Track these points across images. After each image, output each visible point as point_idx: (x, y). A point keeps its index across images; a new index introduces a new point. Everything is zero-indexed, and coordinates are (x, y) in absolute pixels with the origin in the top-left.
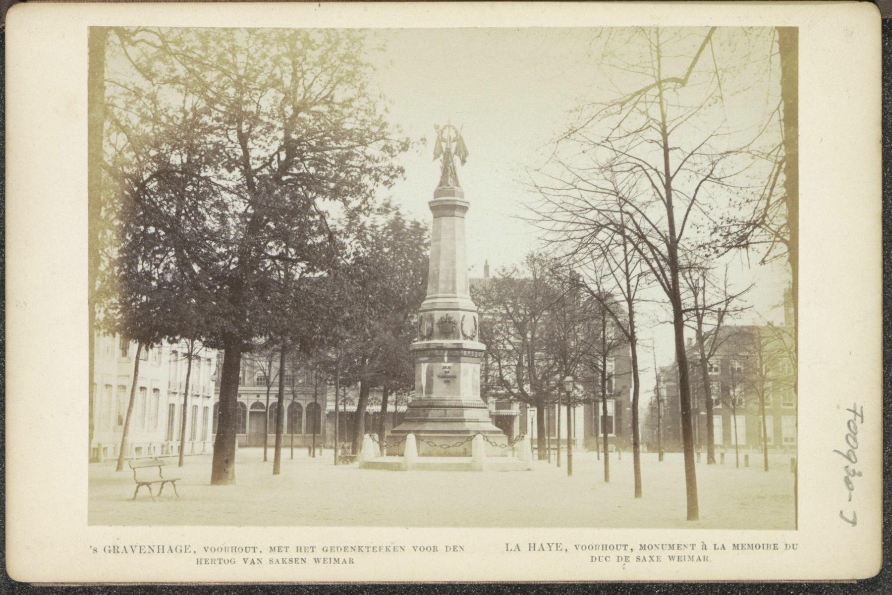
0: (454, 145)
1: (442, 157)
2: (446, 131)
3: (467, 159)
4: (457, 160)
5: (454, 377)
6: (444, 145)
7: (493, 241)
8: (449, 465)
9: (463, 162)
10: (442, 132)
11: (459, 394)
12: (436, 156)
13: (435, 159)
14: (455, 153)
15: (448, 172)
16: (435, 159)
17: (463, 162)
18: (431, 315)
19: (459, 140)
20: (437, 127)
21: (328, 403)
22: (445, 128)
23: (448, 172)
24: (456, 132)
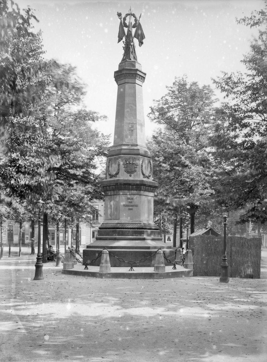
0: (134, 30)
1: (124, 39)
2: (128, 18)
3: (144, 41)
4: (136, 41)
5: (137, 206)
6: (126, 30)
7: (135, 22)
8: (115, 248)
9: (141, 43)
10: (125, 19)
11: (140, 219)
12: (120, 39)
13: (119, 41)
14: (135, 36)
15: (128, 50)
16: (119, 41)
17: (141, 43)
18: (166, 232)
19: (138, 26)
20: (119, 15)
21: (62, 236)
22: (127, 15)
23: (128, 50)
24: (136, 20)
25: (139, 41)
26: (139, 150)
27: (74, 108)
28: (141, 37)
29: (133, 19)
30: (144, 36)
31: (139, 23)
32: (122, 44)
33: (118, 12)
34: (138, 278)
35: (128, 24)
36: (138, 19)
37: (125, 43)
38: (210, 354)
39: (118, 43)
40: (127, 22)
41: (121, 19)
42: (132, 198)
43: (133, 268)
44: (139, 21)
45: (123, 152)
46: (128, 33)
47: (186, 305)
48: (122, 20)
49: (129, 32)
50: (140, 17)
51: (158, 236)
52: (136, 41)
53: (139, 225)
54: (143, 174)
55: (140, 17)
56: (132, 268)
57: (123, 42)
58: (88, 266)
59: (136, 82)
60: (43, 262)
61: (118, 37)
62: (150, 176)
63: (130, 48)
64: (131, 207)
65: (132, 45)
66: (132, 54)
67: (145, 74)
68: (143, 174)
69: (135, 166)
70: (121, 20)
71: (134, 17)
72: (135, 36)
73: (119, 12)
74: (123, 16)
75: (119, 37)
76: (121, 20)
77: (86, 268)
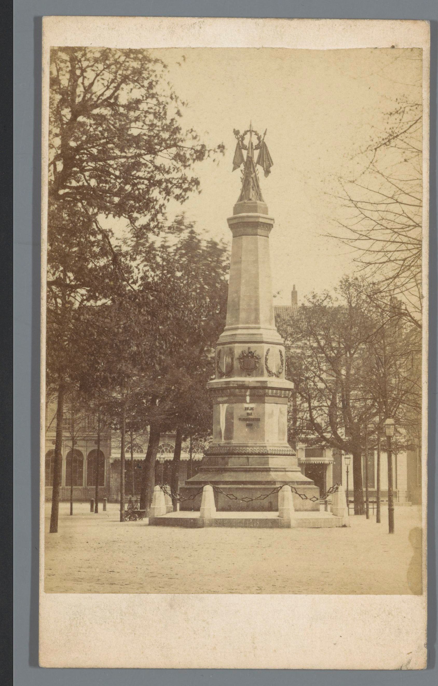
0: (256, 153)
1: (242, 167)
2: (247, 137)
3: (272, 169)
4: (260, 170)
6: (245, 153)
9: (267, 172)
10: (243, 138)
12: (236, 166)
13: (234, 169)
14: (258, 162)
15: (249, 183)
16: (234, 169)
17: (267, 172)
19: (262, 146)
24: (259, 138)
25: (264, 169)
26: (261, 334)
27: (156, 270)
28: (266, 160)
30: (272, 162)
31: (264, 143)
32: (239, 174)
33: (234, 130)
34: (149, 498)
37: (243, 172)
38: (120, 89)
40: (246, 142)
42: (251, 408)
45: (238, 339)
46: (247, 160)
47: (180, 506)
49: (250, 159)
50: (265, 134)
52: (260, 170)
55: (265, 134)
57: (241, 171)
59: (258, 234)
61: (233, 163)
62: (280, 373)
63: (249, 182)
64: (251, 423)
65: (252, 178)
66: (253, 190)
67: (273, 220)
69: (257, 360)
71: (256, 134)
72: (258, 162)
73: (236, 130)
74: (241, 133)
75: (234, 163)
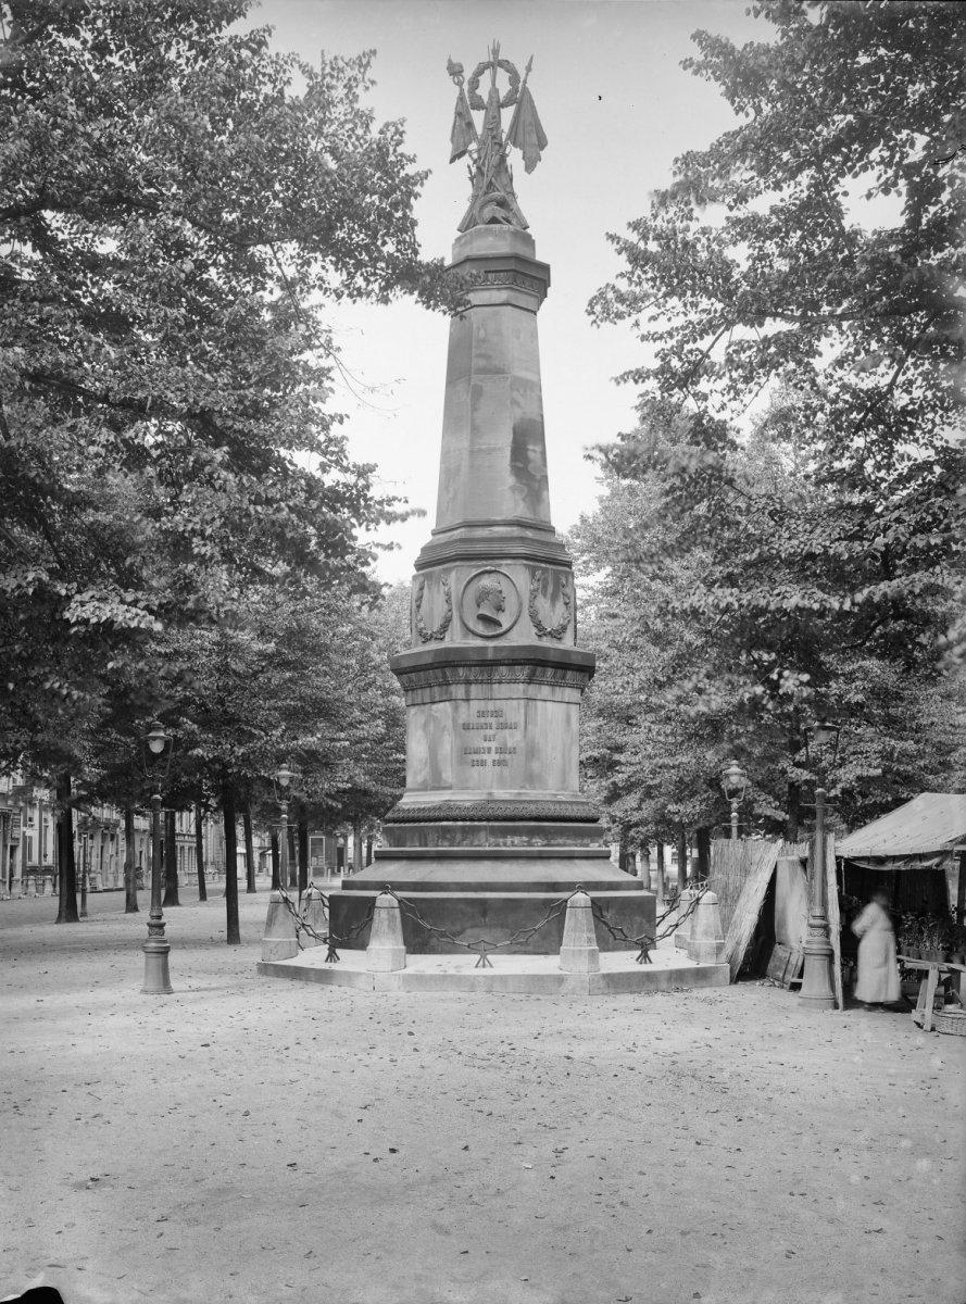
4: (515, 157)
6: (478, 118)
10: (474, 84)
19: (520, 98)
20: (455, 71)
28: (532, 138)
29: (503, 78)
35: (486, 99)
36: (522, 73)
39: (452, 161)
41: (460, 84)
43: (489, 957)
44: (525, 82)
48: (466, 87)
50: (529, 69)
51: (530, 845)
53: (581, 807)
54: (538, 625)
55: (529, 69)
56: (484, 957)
58: (338, 951)
60: (853, 788)
68: (538, 625)
70: (462, 91)
74: (468, 74)
76: (462, 91)
77: (332, 956)
